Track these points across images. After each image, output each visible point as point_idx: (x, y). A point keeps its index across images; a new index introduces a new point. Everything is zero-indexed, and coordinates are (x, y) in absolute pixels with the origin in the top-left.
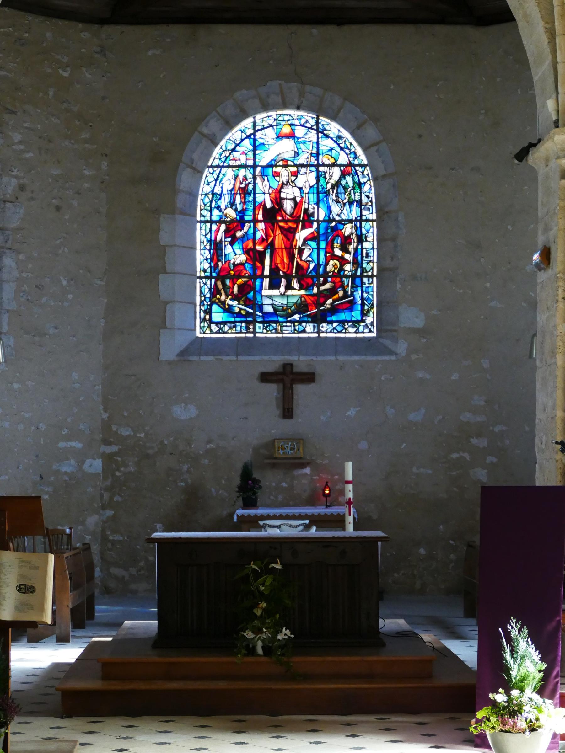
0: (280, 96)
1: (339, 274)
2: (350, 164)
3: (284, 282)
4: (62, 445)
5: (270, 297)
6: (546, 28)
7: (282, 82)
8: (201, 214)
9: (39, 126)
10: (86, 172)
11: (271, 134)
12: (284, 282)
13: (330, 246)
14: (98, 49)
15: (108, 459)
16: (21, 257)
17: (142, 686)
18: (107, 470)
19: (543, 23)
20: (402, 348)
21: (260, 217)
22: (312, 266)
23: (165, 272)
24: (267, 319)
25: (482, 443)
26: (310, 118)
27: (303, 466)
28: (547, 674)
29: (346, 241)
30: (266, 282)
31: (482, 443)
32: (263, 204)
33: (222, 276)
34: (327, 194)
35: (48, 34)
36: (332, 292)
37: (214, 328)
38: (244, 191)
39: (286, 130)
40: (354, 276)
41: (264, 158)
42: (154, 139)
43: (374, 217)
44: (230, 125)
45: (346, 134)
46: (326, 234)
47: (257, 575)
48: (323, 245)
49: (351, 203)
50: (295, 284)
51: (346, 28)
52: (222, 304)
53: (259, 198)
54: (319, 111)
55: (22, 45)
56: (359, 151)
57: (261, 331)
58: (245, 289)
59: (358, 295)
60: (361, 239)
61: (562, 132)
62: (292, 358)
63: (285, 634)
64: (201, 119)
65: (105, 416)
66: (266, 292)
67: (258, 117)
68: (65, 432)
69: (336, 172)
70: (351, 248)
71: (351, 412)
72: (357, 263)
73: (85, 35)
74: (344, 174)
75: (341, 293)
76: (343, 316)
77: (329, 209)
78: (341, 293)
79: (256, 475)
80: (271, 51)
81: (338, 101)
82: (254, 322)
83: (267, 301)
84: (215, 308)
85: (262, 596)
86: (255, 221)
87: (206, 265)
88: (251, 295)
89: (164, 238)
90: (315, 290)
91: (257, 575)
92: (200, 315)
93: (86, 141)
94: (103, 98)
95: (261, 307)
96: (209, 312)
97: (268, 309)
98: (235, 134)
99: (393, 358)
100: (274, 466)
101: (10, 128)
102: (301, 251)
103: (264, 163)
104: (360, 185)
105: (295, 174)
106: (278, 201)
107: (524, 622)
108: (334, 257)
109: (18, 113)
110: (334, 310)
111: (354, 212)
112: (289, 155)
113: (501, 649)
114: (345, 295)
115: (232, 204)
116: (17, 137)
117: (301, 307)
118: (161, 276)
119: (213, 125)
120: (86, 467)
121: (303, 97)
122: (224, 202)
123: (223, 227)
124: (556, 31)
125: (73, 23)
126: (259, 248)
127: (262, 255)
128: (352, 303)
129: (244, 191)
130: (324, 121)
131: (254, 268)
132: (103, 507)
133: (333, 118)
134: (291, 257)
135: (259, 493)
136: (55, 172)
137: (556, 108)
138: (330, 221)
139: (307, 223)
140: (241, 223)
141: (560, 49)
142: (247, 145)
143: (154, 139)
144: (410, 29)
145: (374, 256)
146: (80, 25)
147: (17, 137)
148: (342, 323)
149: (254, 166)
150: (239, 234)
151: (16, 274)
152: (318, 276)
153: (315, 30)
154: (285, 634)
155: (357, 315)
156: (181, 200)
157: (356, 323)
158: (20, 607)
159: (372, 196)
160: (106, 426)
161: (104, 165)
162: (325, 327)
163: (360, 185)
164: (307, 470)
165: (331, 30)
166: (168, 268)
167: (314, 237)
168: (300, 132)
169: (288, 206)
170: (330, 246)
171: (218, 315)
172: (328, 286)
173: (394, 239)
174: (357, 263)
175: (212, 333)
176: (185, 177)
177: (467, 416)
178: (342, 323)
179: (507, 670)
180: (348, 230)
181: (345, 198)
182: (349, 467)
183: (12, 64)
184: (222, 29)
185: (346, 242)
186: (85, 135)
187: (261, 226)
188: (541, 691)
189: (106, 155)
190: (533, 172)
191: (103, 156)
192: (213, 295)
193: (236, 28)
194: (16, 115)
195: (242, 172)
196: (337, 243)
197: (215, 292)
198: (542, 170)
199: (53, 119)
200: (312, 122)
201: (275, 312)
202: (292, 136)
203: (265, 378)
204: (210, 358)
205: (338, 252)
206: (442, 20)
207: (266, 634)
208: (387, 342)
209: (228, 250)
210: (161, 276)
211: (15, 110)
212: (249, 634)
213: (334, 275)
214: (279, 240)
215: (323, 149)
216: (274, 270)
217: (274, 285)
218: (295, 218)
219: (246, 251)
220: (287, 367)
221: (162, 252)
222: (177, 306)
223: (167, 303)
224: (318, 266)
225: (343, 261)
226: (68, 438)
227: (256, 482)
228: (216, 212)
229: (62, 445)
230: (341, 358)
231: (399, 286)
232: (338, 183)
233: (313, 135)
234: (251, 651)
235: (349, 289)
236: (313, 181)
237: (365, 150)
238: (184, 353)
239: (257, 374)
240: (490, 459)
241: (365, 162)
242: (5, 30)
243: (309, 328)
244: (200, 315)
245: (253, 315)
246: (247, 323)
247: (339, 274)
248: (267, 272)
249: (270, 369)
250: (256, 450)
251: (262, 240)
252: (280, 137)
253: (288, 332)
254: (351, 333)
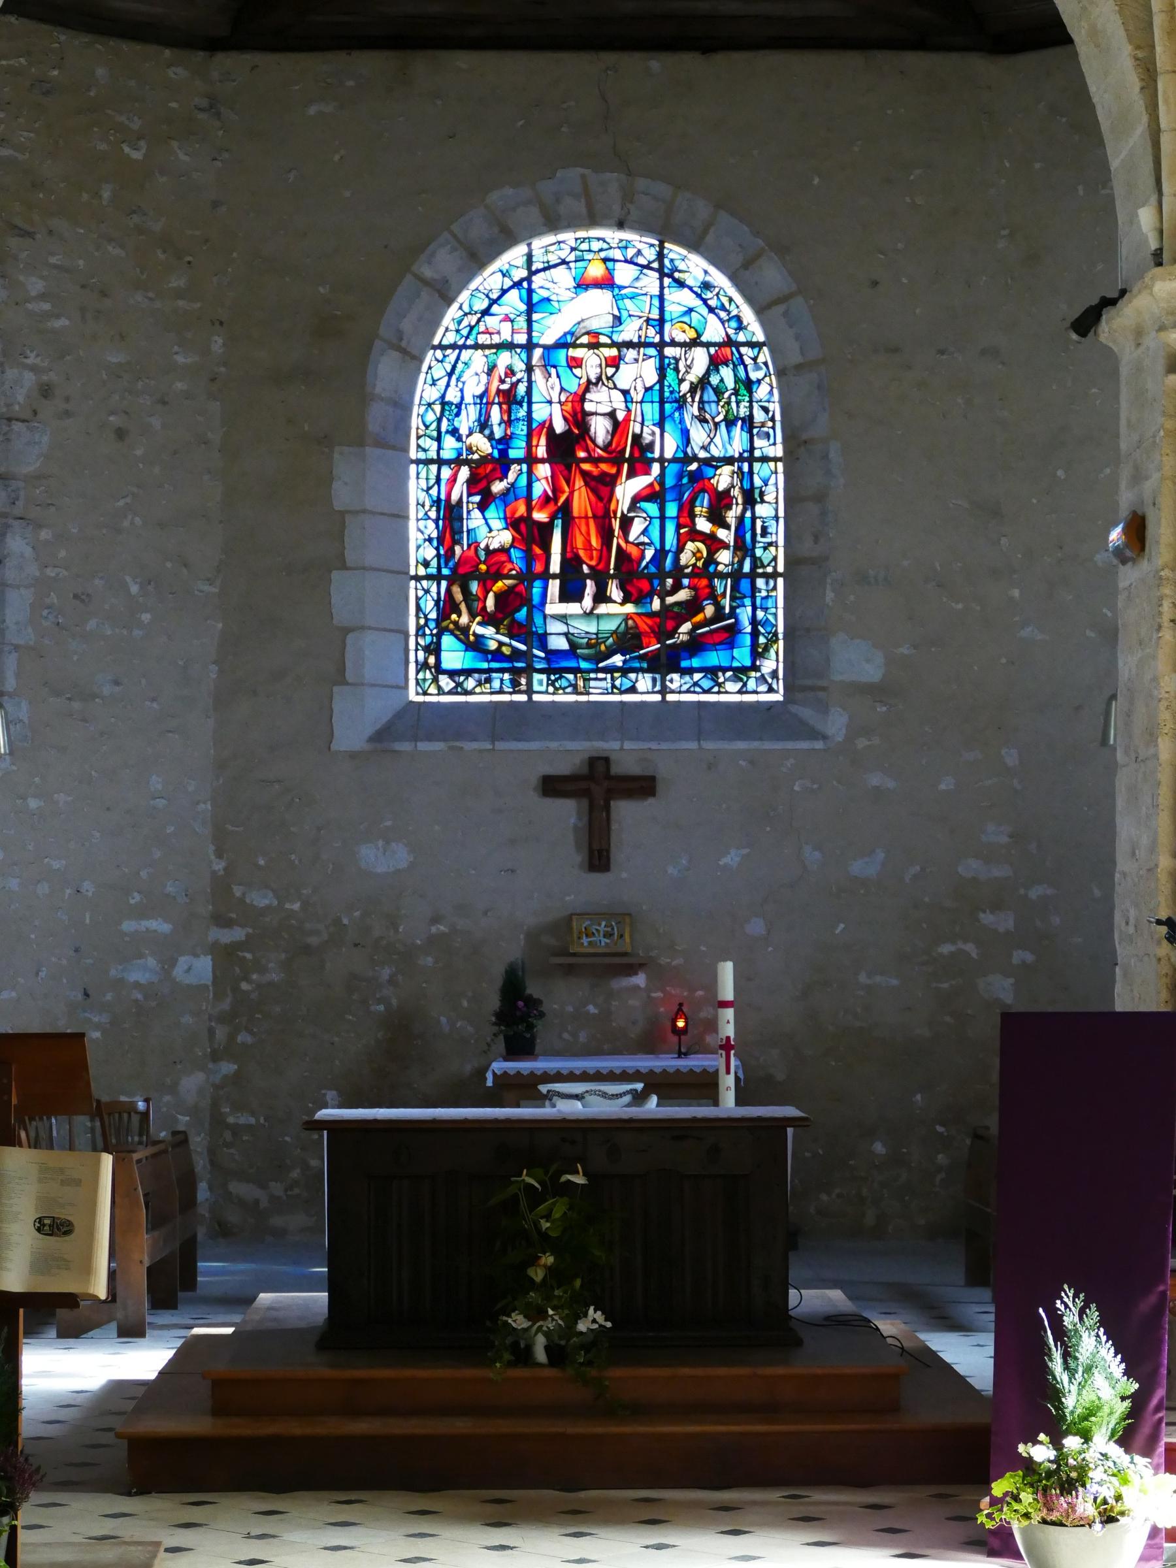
0: (583, 200)
1: (706, 571)
2: (729, 342)
3: (590, 587)
4: (128, 926)
5: (563, 618)
6: (1137, 59)
7: (587, 172)
8: (419, 445)
9: (81, 262)
10: (180, 359)
11: (563, 278)
12: (590, 587)
13: (687, 513)
14: (204, 103)
15: (225, 955)
16: (45, 534)
17: (295, 1428)
18: (224, 979)
19: (1130, 47)
20: (836, 724)
21: (541, 452)
22: (649, 553)
23: (344, 567)
24: (555, 665)
25: (1003, 922)
26: (644, 245)
27: (630, 969)
28: (1138, 1403)
29: (720, 502)
30: (554, 586)
31: (1003, 922)
32: (547, 425)
33: (461, 574)
34: (681, 403)
35: (101, 72)
36: (692, 607)
37: (446, 682)
38: (508, 398)
39: (596, 270)
40: (736, 575)
41: (549, 330)
42: (321, 290)
43: (779, 451)
44: (478, 260)
45: (719, 279)
47: (535, 1197)
48: (672, 509)
49: (730, 423)
50: (615, 592)
51: (720, 58)
52: (462, 633)
53: (540, 413)
54: (664, 232)
55: (47, 93)
56: (748, 315)
57: (543, 690)
58: (509, 602)
59: (745, 614)
60: (751, 498)
61: (1170, 274)
62: (609, 746)
63: (593, 1320)
64: (419, 248)
65: (219, 866)
66: (554, 607)
67: (538, 244)
68: (135, 899)
69: (700, 359)
70: (731, 516)
71: (731, 859)
72: (742, 548)
73: (177, 73)
74: (715, 363)
75: (709, 610)
76: (713, 658)
77: (685, 435)
78: (709, 610)
79: (533, 989)
80: (565, 106)
81: (703, 209)
82: (530, 670)
83: (555, 627)
84: (448, 641)
85: (546, 1242)
86: (531, 460)
87: (429, 553)
88: (522, 614)
89: (342, 496)
90: (656, 604)
91: (535, 1197)
92: (416, 656)
93: (179, 294)
94: (215, 204)
95: (543, 639)
96: (434, 649)
97: (559, 643)
98: (490, 279)
99: (819, 745)
100: (570, 970)
101: (21, 266)
102: (626, 523)
103: (549, 339)
104: (749, 384)
105: (615, 363)
106: (578, 418)
107: (1092, 1295)
108: (695, 535)
109: (38, 236)
110: (696, 645)
111: (738, 442)
112: (601, 323)
113: (1043, 1351)
114: (719, 615)
115: (483, 425)
116: (35, 285)
117: (627, 640)
118: (336, 575)
119: (444, 260)
120: (178, 972)
121: (631, 202)
122: (466, 421)
123: (464, 473)
124: (1158, 65)
125: (152, 49)
126: (540, 516)
127: (546, 530)
128: (734, 631)
129: (508, 398)
130: (674, 251)
131: (529, 558)
132: (215, 1057)
133: (694, 246)
134: (606, 535)
135: (539, 1026)
136: (115, 358)
137: (1158, 225)
138: (687, 459)
139: (639, 465)
140: (502, 464)
141: (1166, 101)
142: (514, 301)
143: (321, 290)
144: (853, 60)
145: (778, 533)
146: (167, 53)
147: (35, 285)
148: (712, 672)
149: (530, 346)
150: (498, 487)
151: (33, 570)
152: (662, 575)
153: (656, 63)
154: (593, 1320)
155: (742, 656)
156: (377, 416)
157: (740, 673)
158: (42, 1264)
159: (775, 408)
160: (221, 887)
161: (217, 344)
162: (676, 680)
163: (749, 384)
164: (640, 980)
165: (689, 63)
166: (351, 557)
167: (653, 494)
168: (624, 274)
169: (600, 429)
170: (687, 513)
171: (454, 655)
172: (683, 595)
173: (820, 498)
174: (742, 548)
175: (441, 693)
176: (385, 368)
177: (971, 867)
178: (712, 672)
179: (1056, 1395)
180: (723, 478)
181: (717, 412)
182: (727, 972)
183: (25, 134)
184: (463, 60)
185: (720, 504)
186: (177, 282)
187: (543, 470)
188: (1126, 1439)
189: (221, 323)
190: (1110, 358)
191: (213, 324)
192: (443, 615)
193: (490, 58)
194: (34, 239)
195: (504, 359)
196: (702, 507)
197: (447, 607)
198: (1127, 354)
199: (110, 248)
200: (650, 254)
201: (573, 650)
202: (607, 282)
203: (552, 786)
204: (438, 746)
205: (703, 525)
206: (921, 42)
207: (554, 1320)
208: (806, 713)
209: (474, 520)
210: (336, 575)
211: (32, 230)
212: (518, 1321)
213: (696, 573)
214: (581, 500)
215: (672, 310)
216: (571, 562)
217: (571, 593)
218: (614, 454)
219: (513, 523)
220: (598, 765)
221: (337, 525)
222: (369, 636)
223: (347, 631)
224: (661, 553)
225: (714, 543)
226: (142, 913)
227: (533, 1003)
228: (449, 442)
229: (128, 926)
230: (709, 745)
231: (830, 595)
232: (703, 382)
233: (651, 281)
234: (523, 1356)
235: (726, 603)
236: (651, 378)
237: (760, 311)
238: (383, 735)
239: (534, 779)
240: (1020, 956)
241: (760, 337)
242: (11, 62)
243: (644, 682)
244: (416, 656)
245: (526, 656)
246: (515, 672)
247: (706, 571)
248: (555, 567)
249: (563, 768)
250: (533, 937)
251: (546, 500)
252: (583, 285)
253: (599, 692)
254: (731, 693)
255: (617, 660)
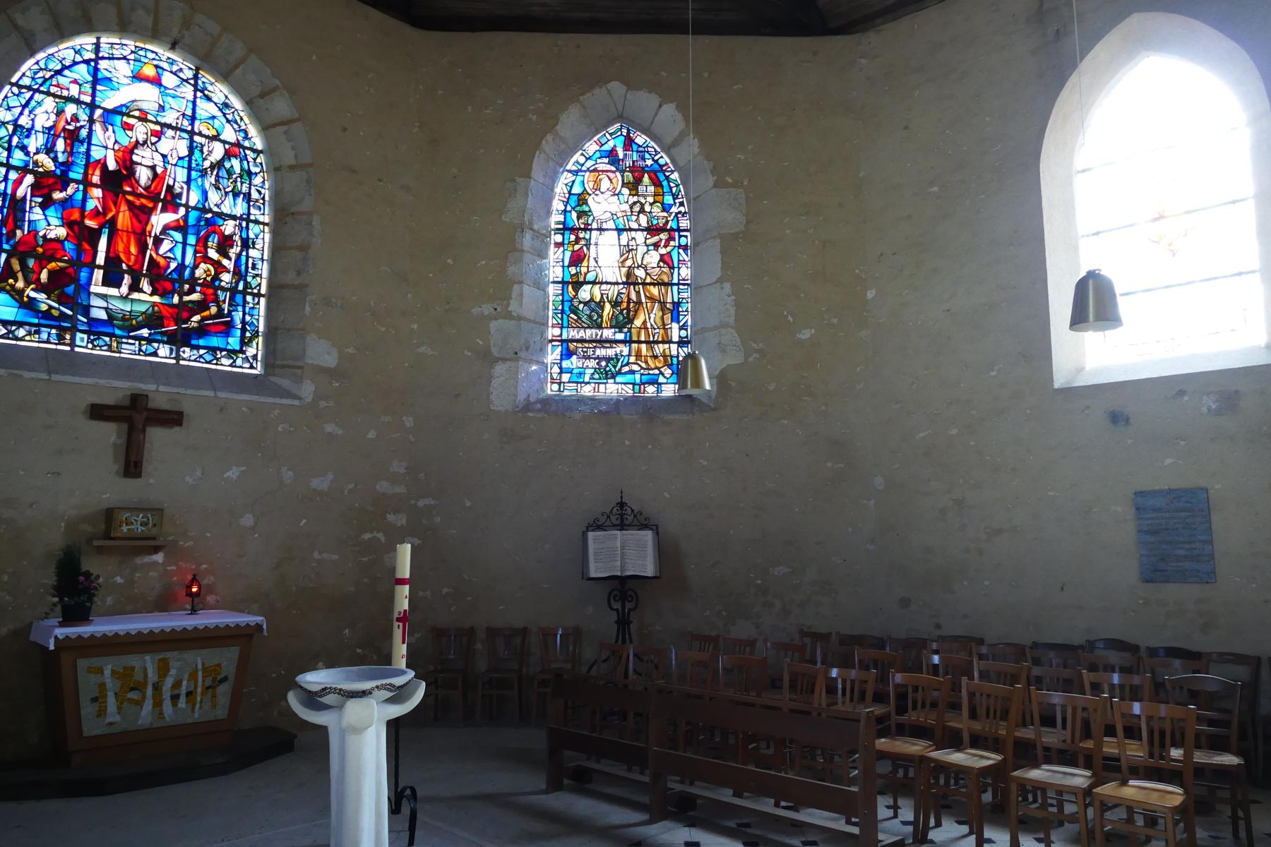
1: (212, 284)
3: (127, 280)
5: (104, 297)
12: (127, 280)
22: (173, 265)
24: (95, 329)
27: (156, 550)
30: (98, 275)
34: (203, 173)
36: (202, 306)
38: (73, 137)
40: (233, 291)
41: (109, 100)
46: (197, 225)
48: (192, 240)
50: (145, 285)
59: (238, 316)
60: (246, 244)
62: (147, 387)
70: (233, 252)
71: (233, 473)
74: (228, 155)
75: (214, 310)
76: (215, 341)
78: (214, 310)
79: (91, 564)
83: (95, 302)
88: (70, 289)
90: (176, 299)
98: (65, 51)
102: (158, 242)
105: (158, 135)
108: (207, 260)
110: (202, 331)
111: (240, 208)
112: (150, 107)
114: (220, 313)
117: (153, 320)
122: (35, 142)
123: (29, 179)
130: (206, 78)
131: (79, 250)
133: (225, 76)
134: (143, 247)
139: (171, 202)
140: (64, 182)
145: (264, 269)
148: (213, 350)
155: (234, 342)
162: (187, 352)
167: (182, 227)
168: (169, 80)
169: (143, 175)
170: (202, 243)
172: (195, 297)
174: (238, 274)
177: (383, 486)
180: (229, 227)
182: (405, 552)
195: (71, 109)
203: (98, 412)
205: (213, 254)
214: (124, 219)
216: (113, 261)
230: (222, 395)
235: (226, 306)
243: (164, 350)
247: (212, 284)
248: (100, 259)
249: (109, 400)
251: (95, 214)
253: (129, 350)
254: (225, 364)
255: (145, 332)
